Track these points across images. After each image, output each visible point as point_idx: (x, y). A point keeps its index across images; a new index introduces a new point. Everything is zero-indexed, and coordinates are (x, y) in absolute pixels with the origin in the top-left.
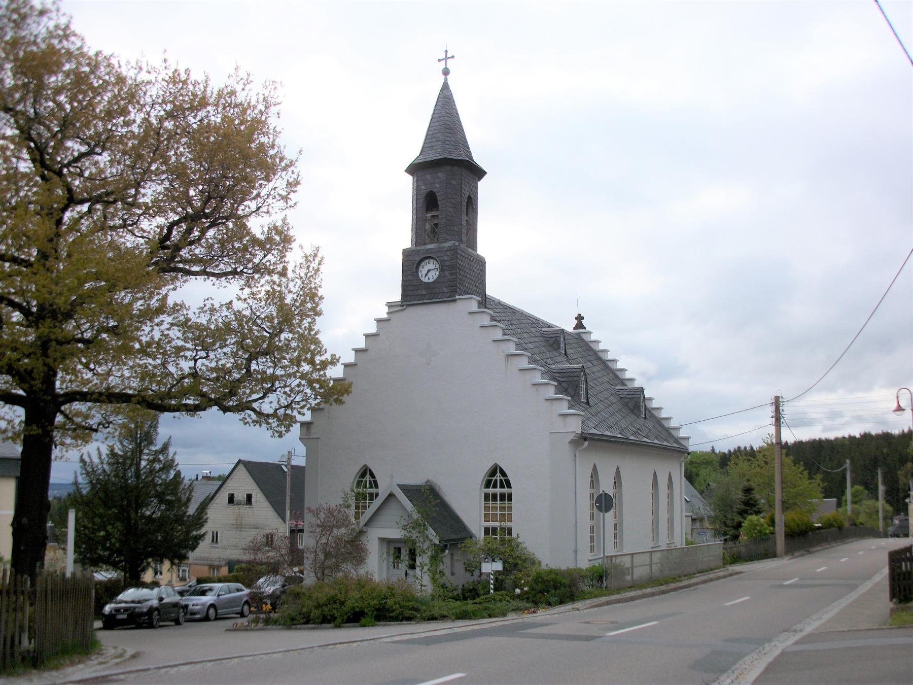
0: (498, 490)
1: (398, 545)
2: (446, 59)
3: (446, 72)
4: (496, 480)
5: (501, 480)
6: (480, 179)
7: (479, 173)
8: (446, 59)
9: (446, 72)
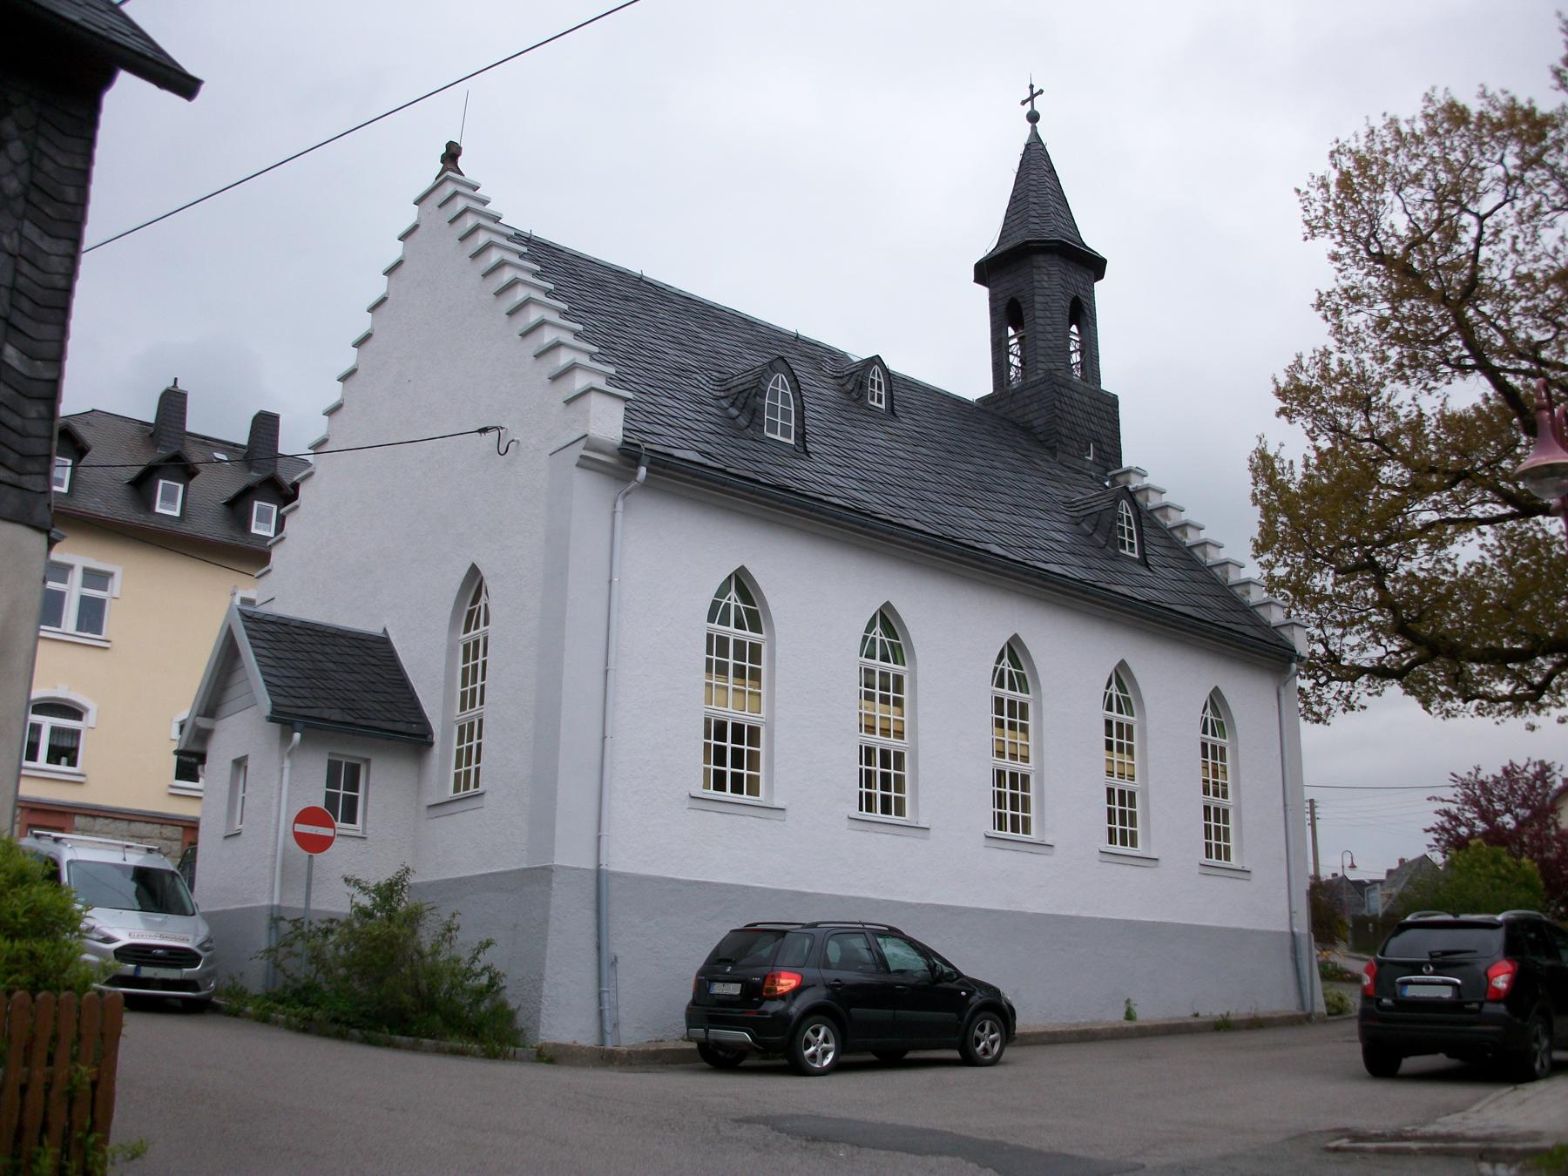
0: (731, 632)
1: (88, 637)
2: (1033, 97)
3: (1033, 117)
4: (727, 605)
5: (737, 608)
6: (1100, 275)
7: (1095, 266)
8: (1033, 97)
9: (1033, 117)
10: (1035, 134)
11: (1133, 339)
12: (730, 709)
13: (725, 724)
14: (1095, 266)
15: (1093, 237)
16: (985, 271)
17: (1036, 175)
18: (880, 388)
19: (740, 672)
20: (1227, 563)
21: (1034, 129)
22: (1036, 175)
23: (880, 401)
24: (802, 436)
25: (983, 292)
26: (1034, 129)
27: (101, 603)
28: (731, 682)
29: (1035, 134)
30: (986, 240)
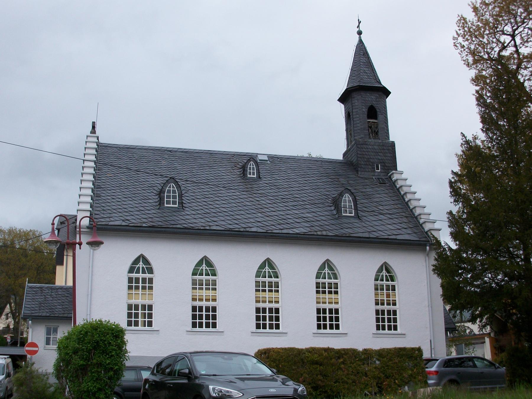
3: (360, 33)
7: (386, 93)
9: (360, 33)
10: (361, 41)
11: (402, 122)
12: (140, 300)
13: (266, 308)
14: (386, 93)
15: (385, 83)
16: (343, 99)
17: (362, 57)
18: (253, 169)
19: (144, 288)
20: (415, 207)
21: (360, 38)
22: (362, 57)
23: (254, 174)
24: (181, 203)
25: (342, 106)
26: (360, 38)
27: (369, 117)
28: (140, 291)
29: (361, 41)
30: (342, 87)
